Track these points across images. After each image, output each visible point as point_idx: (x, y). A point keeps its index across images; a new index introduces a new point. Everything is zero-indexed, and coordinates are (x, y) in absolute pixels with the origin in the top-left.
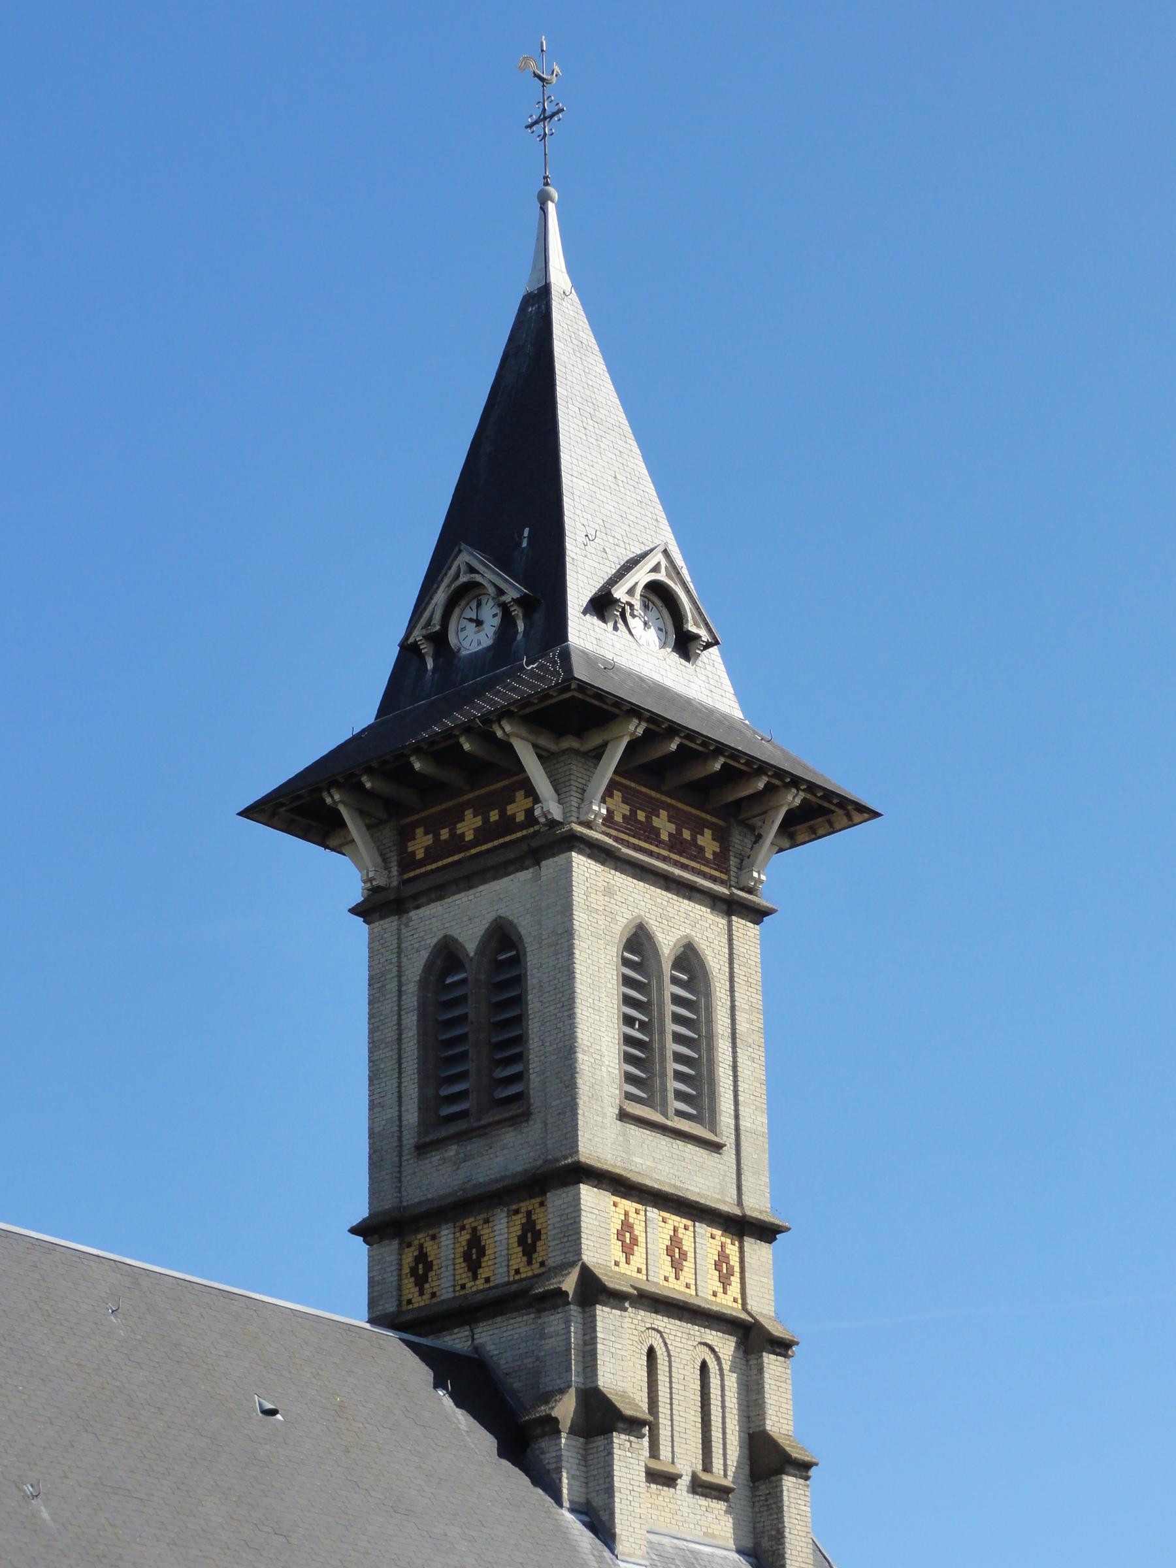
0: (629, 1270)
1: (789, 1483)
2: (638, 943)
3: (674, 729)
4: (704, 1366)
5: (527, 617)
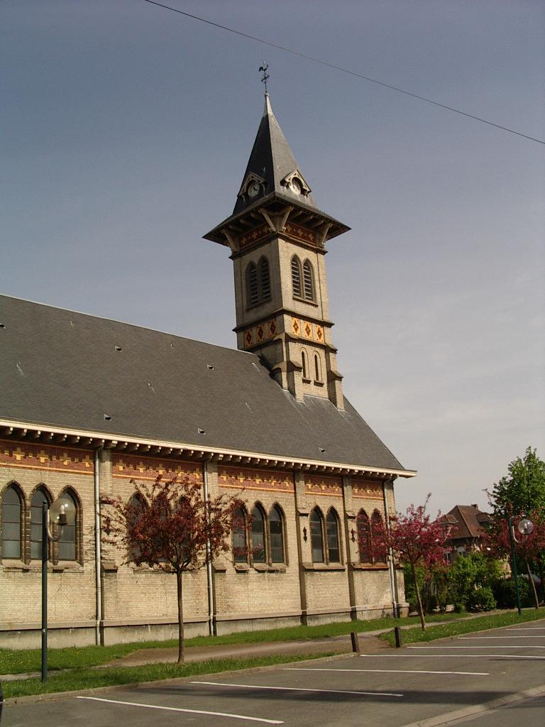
0: (297, 334)
1: (337, 382)
2: (295, 259)
3: (300, 209)
4: (316, 356)
5: (266, 187)
